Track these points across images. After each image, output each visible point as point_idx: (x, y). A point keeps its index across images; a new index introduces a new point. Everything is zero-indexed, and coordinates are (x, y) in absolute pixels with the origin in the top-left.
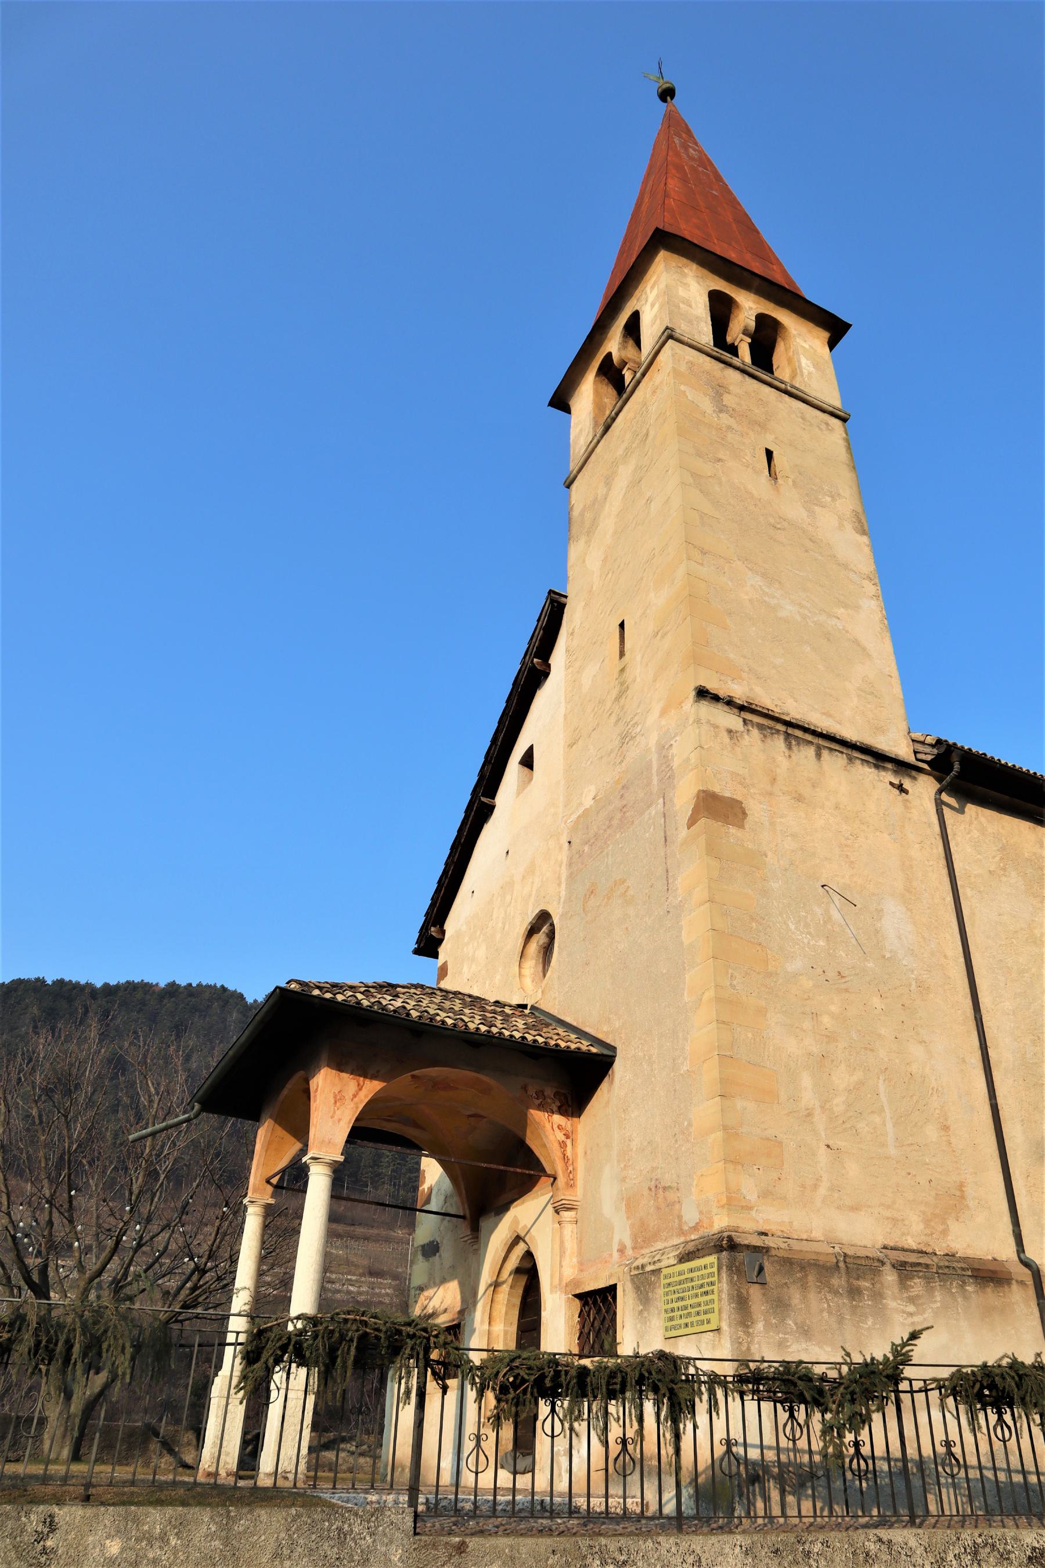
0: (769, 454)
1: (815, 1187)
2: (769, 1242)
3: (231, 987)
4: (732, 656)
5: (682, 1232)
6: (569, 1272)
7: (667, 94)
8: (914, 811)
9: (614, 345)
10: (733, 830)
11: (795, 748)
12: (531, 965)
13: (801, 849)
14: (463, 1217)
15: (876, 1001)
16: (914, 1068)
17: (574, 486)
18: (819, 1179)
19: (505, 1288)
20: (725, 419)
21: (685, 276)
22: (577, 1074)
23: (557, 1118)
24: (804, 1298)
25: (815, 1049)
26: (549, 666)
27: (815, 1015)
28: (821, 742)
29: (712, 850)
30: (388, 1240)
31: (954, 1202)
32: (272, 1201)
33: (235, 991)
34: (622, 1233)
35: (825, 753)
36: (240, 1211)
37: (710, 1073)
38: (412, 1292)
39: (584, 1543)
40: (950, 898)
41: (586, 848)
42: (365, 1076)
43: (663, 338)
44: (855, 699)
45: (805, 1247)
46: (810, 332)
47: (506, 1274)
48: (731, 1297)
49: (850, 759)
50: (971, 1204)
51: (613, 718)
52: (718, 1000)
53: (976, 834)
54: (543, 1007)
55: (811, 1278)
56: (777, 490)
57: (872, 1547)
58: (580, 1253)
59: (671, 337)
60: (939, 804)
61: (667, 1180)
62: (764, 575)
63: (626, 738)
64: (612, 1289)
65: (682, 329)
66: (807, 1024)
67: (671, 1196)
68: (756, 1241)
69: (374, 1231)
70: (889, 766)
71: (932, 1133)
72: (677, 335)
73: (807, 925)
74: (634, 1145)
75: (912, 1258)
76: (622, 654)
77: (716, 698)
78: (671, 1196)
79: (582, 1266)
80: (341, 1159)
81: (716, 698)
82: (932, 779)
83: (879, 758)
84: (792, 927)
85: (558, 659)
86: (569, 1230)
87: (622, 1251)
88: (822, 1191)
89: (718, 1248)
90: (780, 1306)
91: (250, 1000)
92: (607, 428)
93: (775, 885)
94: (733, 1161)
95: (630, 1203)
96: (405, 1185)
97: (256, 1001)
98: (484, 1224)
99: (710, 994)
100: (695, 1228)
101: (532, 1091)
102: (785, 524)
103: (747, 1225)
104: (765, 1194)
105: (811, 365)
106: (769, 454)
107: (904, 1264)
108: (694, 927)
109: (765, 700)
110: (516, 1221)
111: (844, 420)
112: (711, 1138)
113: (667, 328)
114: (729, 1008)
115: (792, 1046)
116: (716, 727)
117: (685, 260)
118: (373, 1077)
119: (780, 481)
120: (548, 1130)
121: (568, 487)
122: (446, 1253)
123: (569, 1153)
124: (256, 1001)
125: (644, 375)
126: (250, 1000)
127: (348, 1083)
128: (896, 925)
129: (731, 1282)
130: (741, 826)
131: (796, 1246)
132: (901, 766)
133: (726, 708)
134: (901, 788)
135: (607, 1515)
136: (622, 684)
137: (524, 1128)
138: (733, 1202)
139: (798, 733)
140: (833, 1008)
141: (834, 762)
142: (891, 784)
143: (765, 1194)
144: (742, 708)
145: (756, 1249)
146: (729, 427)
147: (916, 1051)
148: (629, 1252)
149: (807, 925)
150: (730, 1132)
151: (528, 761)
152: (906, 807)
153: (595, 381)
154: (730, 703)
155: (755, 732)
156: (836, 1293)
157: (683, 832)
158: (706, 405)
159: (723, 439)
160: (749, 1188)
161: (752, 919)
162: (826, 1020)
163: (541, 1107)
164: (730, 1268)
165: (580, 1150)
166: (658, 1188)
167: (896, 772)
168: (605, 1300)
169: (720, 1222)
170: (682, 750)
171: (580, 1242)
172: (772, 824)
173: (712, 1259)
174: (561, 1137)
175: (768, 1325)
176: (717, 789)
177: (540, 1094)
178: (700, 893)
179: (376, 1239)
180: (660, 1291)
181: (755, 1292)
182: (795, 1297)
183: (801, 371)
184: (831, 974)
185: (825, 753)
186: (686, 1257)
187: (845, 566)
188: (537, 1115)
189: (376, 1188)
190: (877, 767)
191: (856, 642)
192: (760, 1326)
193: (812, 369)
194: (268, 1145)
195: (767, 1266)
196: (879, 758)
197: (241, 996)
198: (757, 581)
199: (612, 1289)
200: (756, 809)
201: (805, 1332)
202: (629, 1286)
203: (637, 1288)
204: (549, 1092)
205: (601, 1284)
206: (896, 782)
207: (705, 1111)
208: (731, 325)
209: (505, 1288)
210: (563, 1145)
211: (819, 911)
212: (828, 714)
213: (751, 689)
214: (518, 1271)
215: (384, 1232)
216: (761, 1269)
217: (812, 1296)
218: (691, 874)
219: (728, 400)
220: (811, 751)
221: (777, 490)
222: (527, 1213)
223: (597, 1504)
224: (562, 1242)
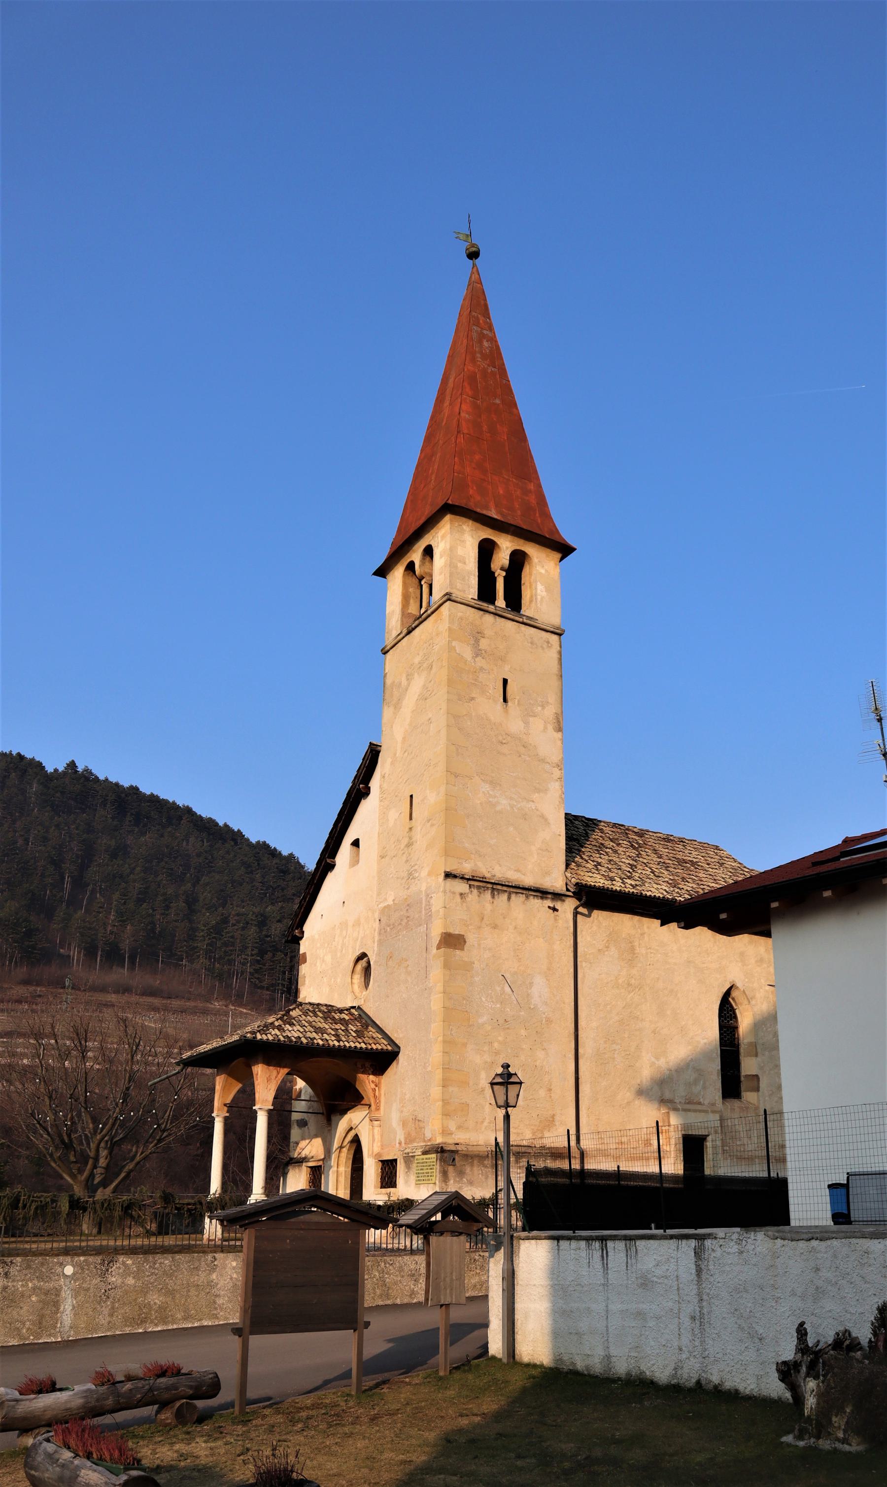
0: (505, 682)
1: (483, 1122)
2: (459, 1148)
3: (28, 755)
4: (467, 845)
5: (425, 1141)
6: (377, 1149)
7: (473, 255)
8: (560, 921)
9: (416, 555)
10: (458, 952)
11: (496, 897)
12: (358, 978)
13: (493, 956)
14: (322, 1114)
15: (523, 1032)
16: (538, 1063)
17: (389, 655)
18: (485, 1119)
19: (345, 1150)
20: (480, 662)
21: (462, 532)
22: (382, 1060)
23: (372, 1077)
24: (472, 1170)
25: (489, 1060)
26: (369, 788)
27: (491, 1043)
28: (512, 890)
29: (447, 966)
30: (205, 1012)
31: (550, 1122)
32: (227, 1115)
33: (33, 759)
34: (400, 1136)
35: (513, 896)
36: (212, 1121)
37: (438, 1075)
38: (292, 1145)
39: (379, 1259)
40: (572, 970)
41: (388, 929)
42: (280, 1067)
43: (444, 599)
44: (536, 856)
45: (475, 1149)
46: (547, 556)
47: (345, 1143)
48: (440, 1171)
49: (527, 897)
50: (557, 1124)
51: (404, 858)
52: (444, 1042)
53: (595, 928)
54: (364, 1009)
55: (475, 1162)
56: (506, 711)
57: (477, 1258)
58: (381, 1141)
59: (449, 600)
60: (576, 913)
61: (420, 1117)
62: (491, 783)
63: (410, 876)
64: (396, 1160)
65: (456, 594)
66: (486, 1048)
67: (421, 1124)
68: (453, 1148)
69: (191, 1004)
70: (550, 896)
71: (542, 1093)
72: (453, 598)
73: (491, 998)
74: (407, 1097)
75: (523, 1149)
76: (411, 818)
77: (455, 877)
78: (421, 1124)
79: (382, 1147)
80: (272, 1108)
81: (455, 877)
82: (574, 899)
83: (542, 893)
84: (484, 999)
85: (375, 783)
86: (376, 1130)
87: (400, 1143)
88: (485, 1124)
89: (437, 1152)
90: (461, 1174)
91: (50, 769)
92: (409, 633)
93: (477, 979)
94: (446, 1114)
95: (404, 1124)
96: (220, 958)
97: (56, 770)
98: (334, 1118)
99: (441, 1038)
100: (430, 1140)
101: (359, 1065)
102: (509, 738)
103: (449, 1141)
104: (459, 1127)
105: (544, 590)
106: (505, 682)
107: (519, 1153)
108: (436, 1003)
109: (485, 869)
110: (350, 1120)
111: (560, 635)
112: (438, 1104)
113: (447, 594)
114: (448, 1043)
115: (478, 1060)
116: (454, 893)
117: (464, 519)
118: (284, 1067)
119: (509, 703)
120: (367, 1082)
121: (385, 653)
122: (312, 1125)
123: (377, 1094)
124: (56, 770)
125: (433, 613)
126: (50, 769)
127: (273, 1071)
128: (539, 989)
129: (441, 1165)
130: (463, 949)
131: (470, 1149)
132: (558, 896)
133: (460, 881)
134: (555, 909)
135: (387, 1249)
136: (410, 838)
137: (355, 1082)
138: (445, 1132)
139: (499, 887)
140: (500, 1038)
141: (518, 900)
142: (549, 907)
143: (459, 1127)
144: (468, 880)
145: (452, 1151)
146: (482, 669)
147: (540, 1054)
148: (403, 1145)
149: (491, 998)
150: (445, 1102)
151: (356, 843)
152: (556, 920)
153: (404, 575)
154: (463, 878)
155: (475, 891)
156: (486, 1167)
157: (434, 951)
158: (467, 653)
159: (476, 680)
160: (452, 1126)
161: (464, 999)
162: (496, 1045)
163: (363, 1073)
164: (440, 1160)
165: (382, 1092)
166: (416, 1120)
167: (553, 899)
168: (392, 1164)
169: (439, 1140)
170: (437, 903)
171: (382, 1136)
172: (479, 945)
173: (434, 1156)
174: (373, 1086)
175: (455, 1181)
176: (452, 931)
177: (363, 1066)
178: (440, 987)
179: (194, 1012)
180: (415, 1165)
181: (451, 1169)
182: (468, 1169)
183: (536, 599)
184: (501, 1021)
185: (513, 896)
186: (425, 1153)
187: (543, 761)
188: (361, 1077)
189: (191, 961)
190: (542, 898)
191: (542, 816)
192: (452, 1182)
193: (544, 594)
194: (224, 1088)
195: (457, 1158)
196: (542, 893)
197: (40, 766)
198: (486, 787)
199: (396, 1160)
200: (471, 938)
201: (471, 1183)
202: (402, 1160)
203: (405, 1162)
204: (367, 1064)
205: (391, 1158)
206: (552, 906)
207: (436, 1091)
208: (494, 556)
209: (345, 1150)
210: (374, 1090)
211: (498, 989)
212: (518, 871)
213: (476, 865)
214: (352, 1142)
215: (201, 1005)
216: (454, 1159)
217: (475, 1168)
218: (436, 973)
219: (484, 644)
220: (505, 897)
221: (506, 711)
222: (354, 1117)
223: (390, 1246)
224: (373, 1135)
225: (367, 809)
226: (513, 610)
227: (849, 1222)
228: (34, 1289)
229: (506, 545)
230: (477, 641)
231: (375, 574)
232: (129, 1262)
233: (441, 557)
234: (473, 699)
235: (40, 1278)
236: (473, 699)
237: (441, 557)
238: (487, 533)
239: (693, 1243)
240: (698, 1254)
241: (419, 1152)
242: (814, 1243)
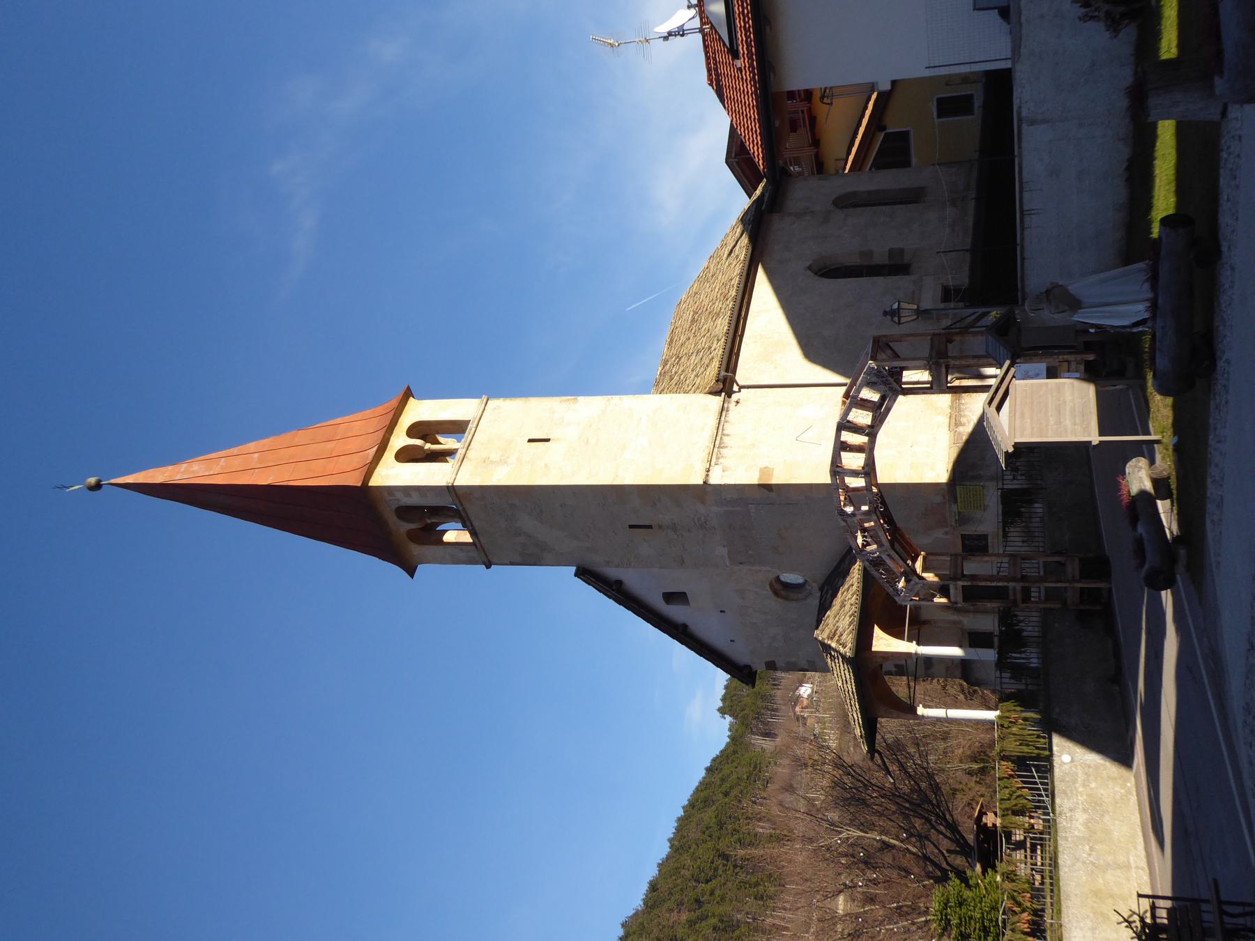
10: (775, 473)
76: (650, 527)
87: (946, 533)
141: (728, 429)
154: (708, 471)
219: (495, 456)
220: (726, 439)
225: (633, 579)
226: (464, 432)
227: (1008, 7)
228: (1084, 786)
229: (400, 440)
230: (491, 462)
231: (412, 575)
232: (1057, 710)
233: (440, 443)
234: (546, 465)
235: (1075, 781)
236: (546, 465)
237: (440, 443)
238: (389, 455)
239: (1025, 127)
240: (1032, 123)
241: (954, 508)
242: (1023, 19)
